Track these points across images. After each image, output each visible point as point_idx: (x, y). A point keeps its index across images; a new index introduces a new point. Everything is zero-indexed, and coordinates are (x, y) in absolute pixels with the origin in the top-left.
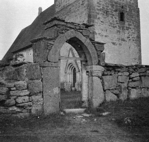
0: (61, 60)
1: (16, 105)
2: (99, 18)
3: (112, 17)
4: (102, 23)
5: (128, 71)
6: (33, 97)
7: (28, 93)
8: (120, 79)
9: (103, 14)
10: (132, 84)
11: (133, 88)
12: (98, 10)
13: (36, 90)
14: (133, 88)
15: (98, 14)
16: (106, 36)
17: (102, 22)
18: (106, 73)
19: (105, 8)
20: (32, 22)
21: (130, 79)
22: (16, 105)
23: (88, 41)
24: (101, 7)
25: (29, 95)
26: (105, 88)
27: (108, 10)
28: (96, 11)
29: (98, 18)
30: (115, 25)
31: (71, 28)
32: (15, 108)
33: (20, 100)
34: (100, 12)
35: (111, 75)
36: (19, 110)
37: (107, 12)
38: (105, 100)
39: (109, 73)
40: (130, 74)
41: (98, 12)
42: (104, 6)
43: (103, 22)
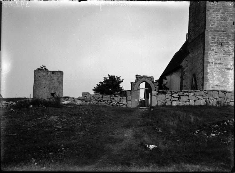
0: (140, 90)
1: (122, 103)
2: (213, 50)
3: (228, 47)
4: (216, 53)
5: (171, 93)
6: (128, 102)
7: (126, 100)
8: (167, 97)
9: (218, 46)
10: (173, 99)
11: (174, 101)
12: (212, 43)
13: (129, 99)
14: (174, 101)
15: (213, 46)
16: (220, 64)
17: (215, 52)
18: (158, 94)
19: (220, 40)
20: (182, 46)
21: (172, 97)
22: (122, 103)
23: (151, 82)
24: (216, 41)
25: (127, 101)
26: (87, 97)
27: (223, 41)
28: (210, 45)
29: (212, 50)
30: (230, 53)
31: (143, 78)
32: (122, 104)
33: (123, 102)
34: (214, 45)
35: (162, 95)
36: (123, 105)
37: (222, 44)
38: (158, 105)
39: (160, 94)
40: (172, 95)
41: (212, 45)
42: (219, 39)
43: (217, 53)
